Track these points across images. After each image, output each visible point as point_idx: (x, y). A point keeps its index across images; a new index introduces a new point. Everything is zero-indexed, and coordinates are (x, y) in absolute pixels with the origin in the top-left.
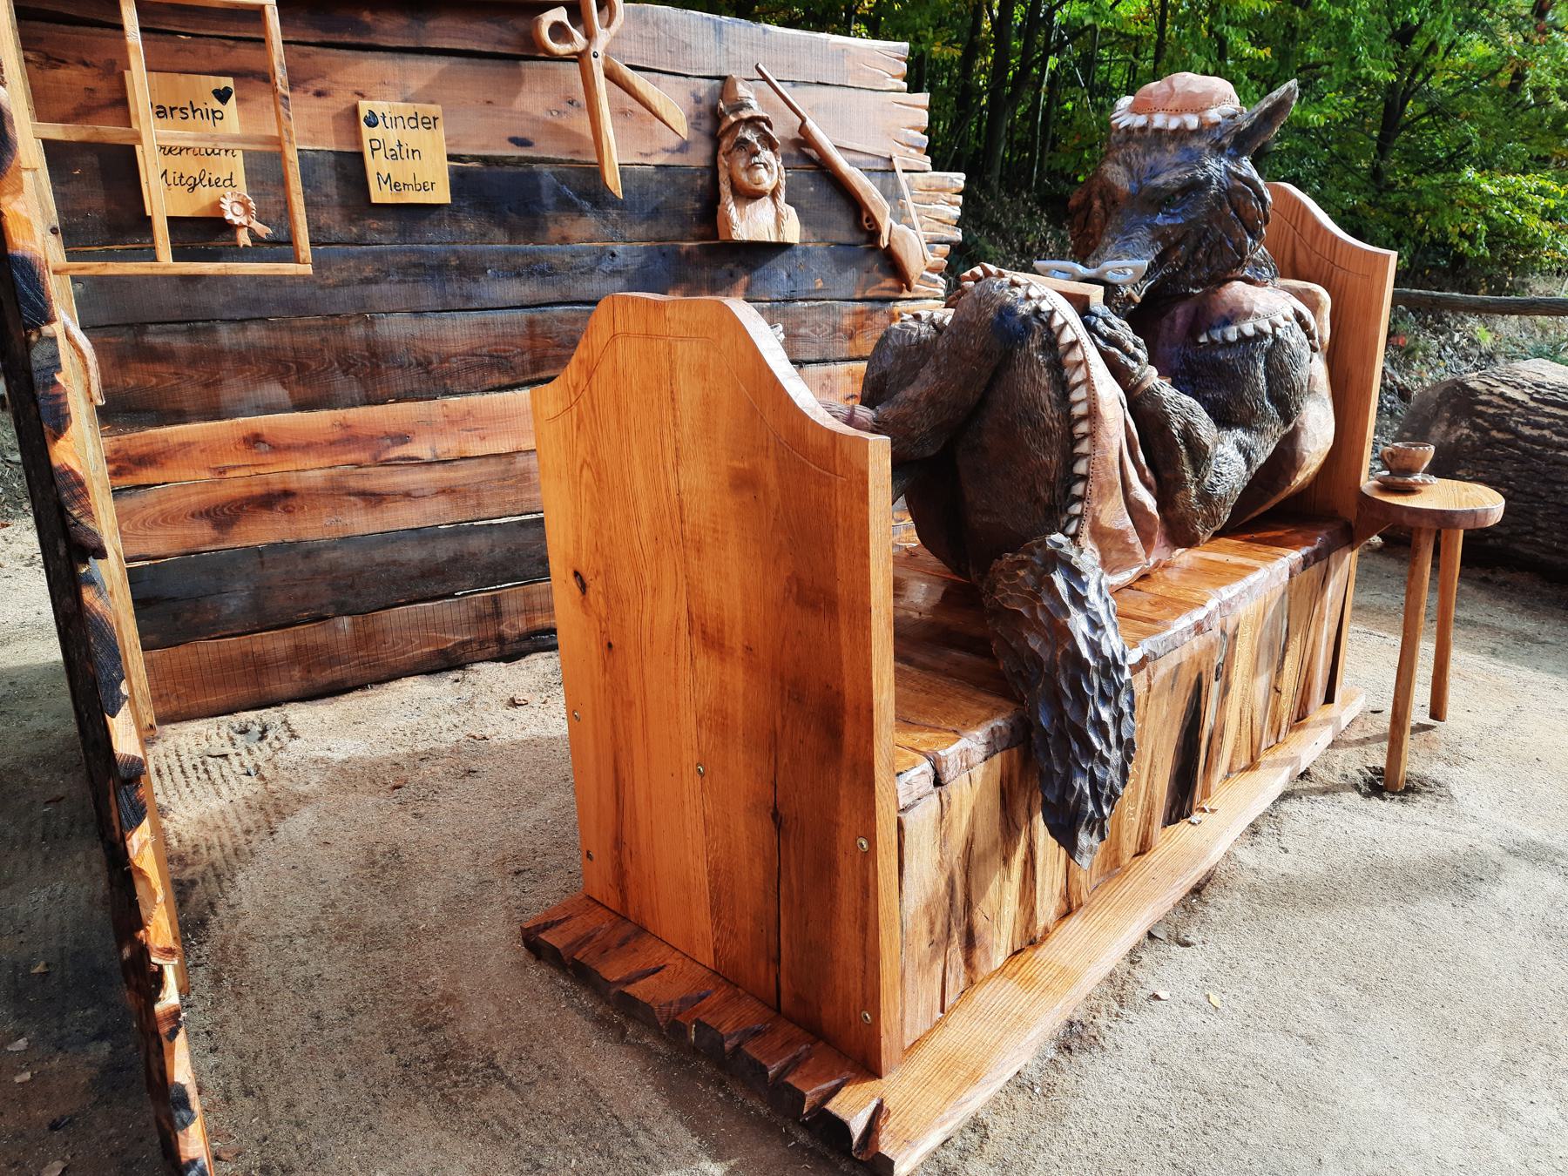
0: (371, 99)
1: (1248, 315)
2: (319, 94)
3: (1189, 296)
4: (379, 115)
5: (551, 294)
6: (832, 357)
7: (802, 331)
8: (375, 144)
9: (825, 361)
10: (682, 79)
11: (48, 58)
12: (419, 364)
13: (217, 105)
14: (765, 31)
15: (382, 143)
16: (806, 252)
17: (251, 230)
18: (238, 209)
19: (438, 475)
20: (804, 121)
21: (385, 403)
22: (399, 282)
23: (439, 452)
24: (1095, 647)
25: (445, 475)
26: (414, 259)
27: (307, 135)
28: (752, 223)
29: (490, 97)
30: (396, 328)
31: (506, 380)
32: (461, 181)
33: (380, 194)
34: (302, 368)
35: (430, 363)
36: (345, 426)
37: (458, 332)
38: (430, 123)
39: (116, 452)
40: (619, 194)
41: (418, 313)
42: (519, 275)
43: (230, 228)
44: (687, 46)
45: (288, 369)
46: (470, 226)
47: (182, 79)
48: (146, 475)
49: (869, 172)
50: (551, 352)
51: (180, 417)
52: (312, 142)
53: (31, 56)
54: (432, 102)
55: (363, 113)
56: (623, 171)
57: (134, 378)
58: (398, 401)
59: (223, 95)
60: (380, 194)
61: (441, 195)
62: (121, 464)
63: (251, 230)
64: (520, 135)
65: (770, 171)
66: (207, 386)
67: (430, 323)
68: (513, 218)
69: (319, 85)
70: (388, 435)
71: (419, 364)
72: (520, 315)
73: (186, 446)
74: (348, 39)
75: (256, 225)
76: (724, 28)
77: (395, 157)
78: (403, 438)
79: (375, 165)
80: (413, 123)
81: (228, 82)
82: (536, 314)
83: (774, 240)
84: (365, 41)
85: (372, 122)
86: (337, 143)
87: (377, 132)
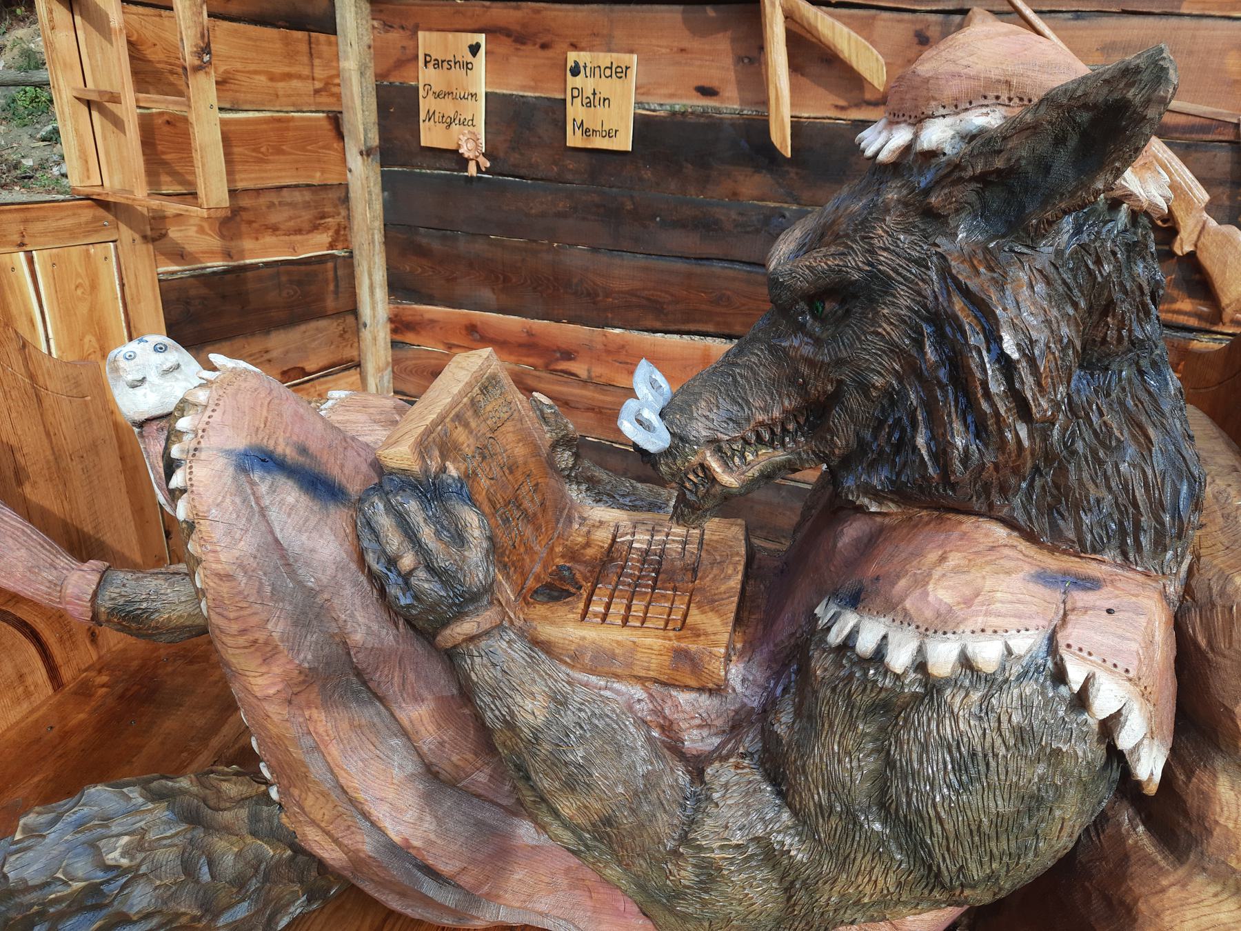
0: (582, 49)
1: (891, 608)
2: (544, 46)
3: (861, 510)
4: (581, 65)
5: (712, 249)
8: (576, 93)
10: (907, 16)
11: (385, 24)
12: (589, 294)
13: (469, 57)
15: (581, 91)
17: (478, 164)
18: (471, 145)
19: (588, 393)
21: (558, 321)
22: (584, 219)
23: (593, 375)
24: (905, 817)
25: (597, 396)
26: (597, 199)
27: (532, 84)
29: (685, 44)
30: (577, 258)
31: (658, 325)
32: (644, 126)
33: (574, 139)
34: (506, 280)
35: (597, 295)
36: (530, 334)
37: (624, 272)
38: (621, 72)
39: (396, 316)
40: (788, 153)
41: (595, 250)
42: (684, 226)
43: (463, 162)
45: (497, 278)
46: (647, 174)
47: (450, 35)
48: (410, 337)
50: (704, 307)
51: (430, 301)
52: (534, 89)
53: (376, 23)
54: (631, 52)
55: (570, 64)
56: (797, 127)
57: (408, 266)
58: (569, 322)
59: (474, 49)
60: (574, 139)
61: (624, 142)
62: (400, 326)
63: (478, 164)
64: (706, 83)
66: (448, 280)
67: (603, 259)
68: (689, 169)
69: (545, 39)
70: (559, 349)
71: (589, 294)
72: (680, 265)
73: (432, 322)
75: (482, 160)
77: (589, 105)
78: (568, 355)
79: (575, 111)
80: (608, 72)
81: (481, 38)
82: (697, 269)
85: (575, 72)
86: (743, 102)
87: (578, 81)
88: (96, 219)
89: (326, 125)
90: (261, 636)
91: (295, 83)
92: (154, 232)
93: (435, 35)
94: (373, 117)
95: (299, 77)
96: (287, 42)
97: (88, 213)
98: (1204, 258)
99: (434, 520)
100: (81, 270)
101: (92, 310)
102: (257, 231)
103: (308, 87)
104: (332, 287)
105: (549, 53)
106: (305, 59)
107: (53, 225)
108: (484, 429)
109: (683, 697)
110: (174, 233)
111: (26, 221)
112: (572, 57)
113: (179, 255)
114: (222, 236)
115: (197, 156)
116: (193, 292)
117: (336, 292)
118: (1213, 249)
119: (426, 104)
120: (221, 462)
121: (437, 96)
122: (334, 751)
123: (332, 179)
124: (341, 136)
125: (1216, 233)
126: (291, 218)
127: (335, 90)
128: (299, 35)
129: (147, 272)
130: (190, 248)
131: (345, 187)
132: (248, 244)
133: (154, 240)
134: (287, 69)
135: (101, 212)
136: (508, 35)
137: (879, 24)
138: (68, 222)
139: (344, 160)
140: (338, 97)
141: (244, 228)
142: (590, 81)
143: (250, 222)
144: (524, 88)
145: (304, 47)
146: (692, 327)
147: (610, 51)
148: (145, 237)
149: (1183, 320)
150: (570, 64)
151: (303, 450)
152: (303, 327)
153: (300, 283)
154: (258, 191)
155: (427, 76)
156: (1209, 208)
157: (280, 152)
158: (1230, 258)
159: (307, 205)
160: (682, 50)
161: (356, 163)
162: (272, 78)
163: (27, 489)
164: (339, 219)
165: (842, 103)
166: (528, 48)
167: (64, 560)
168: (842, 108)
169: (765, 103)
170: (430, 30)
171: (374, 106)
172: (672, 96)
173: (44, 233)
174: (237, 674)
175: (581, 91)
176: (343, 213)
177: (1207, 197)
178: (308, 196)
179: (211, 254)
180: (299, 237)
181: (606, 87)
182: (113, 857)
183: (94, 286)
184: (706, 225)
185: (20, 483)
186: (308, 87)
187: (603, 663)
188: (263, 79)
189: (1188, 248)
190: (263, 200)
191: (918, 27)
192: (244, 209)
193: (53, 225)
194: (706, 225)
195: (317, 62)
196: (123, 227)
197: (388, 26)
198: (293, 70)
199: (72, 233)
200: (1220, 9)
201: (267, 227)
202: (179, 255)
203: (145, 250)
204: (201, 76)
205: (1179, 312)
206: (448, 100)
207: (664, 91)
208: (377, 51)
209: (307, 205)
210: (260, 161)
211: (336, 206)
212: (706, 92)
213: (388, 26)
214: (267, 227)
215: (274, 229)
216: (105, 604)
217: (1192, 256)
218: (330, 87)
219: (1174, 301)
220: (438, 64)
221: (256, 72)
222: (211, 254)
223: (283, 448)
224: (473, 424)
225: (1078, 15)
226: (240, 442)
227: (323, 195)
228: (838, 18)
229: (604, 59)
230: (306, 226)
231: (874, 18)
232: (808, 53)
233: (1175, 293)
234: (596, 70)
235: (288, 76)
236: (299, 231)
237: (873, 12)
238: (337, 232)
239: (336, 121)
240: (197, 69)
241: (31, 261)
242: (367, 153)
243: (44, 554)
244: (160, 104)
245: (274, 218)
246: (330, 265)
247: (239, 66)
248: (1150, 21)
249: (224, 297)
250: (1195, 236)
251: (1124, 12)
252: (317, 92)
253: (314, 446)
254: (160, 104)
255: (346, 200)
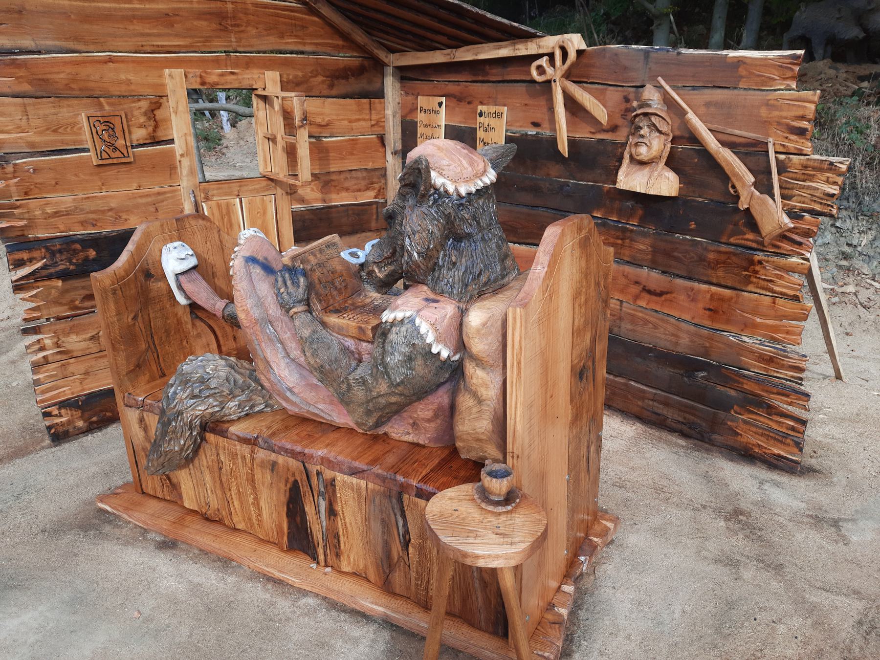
2: (469, 103)
6: (697, 277)
7: (676, 254)
9: (690, 279)
10: (620, 89)
13: (438, 108)
14: (679, 53)
15: (483, 124)
16: (686, 203)
20: (685, 113)
28: (631, 180)
29: (526, 102)
31: (515, 239)
38: (499, 115)
44: (625, 68)
49: (743, 157)
52: (464, 123)
54: (505, 105)
56: (572, 142)
59: (440, 104)
64: (535, 121)
65: (654, 145)
72: (525, 210)
74: (480, 78)
76: (652, 55)
77: (486, 131)
81: (444, 99)
83: (642, 191)
84: (485, 79)
85: (481, 115)
88: (267, 185)
89: (376, 141)
90: (245, 308)
91: (362, 123)
92: (291, 191)
93: (425, 98)
94: (399, 136)
95: (364, 120)
96: (359, 105)
97: (265, 183)
98: (752, 210)
99: (291, 279)
100: (260, 206)
101: (263, 223)
102: (338, 190)
103: (369, 124)
104: (375, 217)
105: (471, 106)
106: (368, 112)
107: (250, 187)
108: (323, 258)
109: (364, 344)
110: (300, 191)
111: (240, 186)
112: (480, 108)
113: (302, 201)
114: (322, 193)
115: (299, 161)
116: (307, 217)
117: (377, 219)
118: (757, 207)
119: (420, 130)
120: (242, 260)
121: (425, 126)
122: (263, 345)
123: (378, 165)
124: (384, 145)
125: (759, 198)
126: (355, 184)
127: (382, 124)
128: (365, 101)
129: (287, 208)
130: (307, 197)
131: (385, 169)
132: (334, 196)
133: (291, 194)
134: (358, 117)
135: (270, 182)
136: (455, 98)
137: (608, 92)
138: (256, 187)
139: (385, 157)
140: (384, 127)
141: (332, 189)
142: (487, 119)
143: (335, 186)
144: (460, 122)
145: (368, 106)
146: (527, 241)
147: (496, 105)
148: (287, 193)
149: (749, 244)
150: (479, 111)
151: (266, 259)
152: (359, 235)
153: (358, 215)
154: (340, 172)
155: (421, 117)
156: (755, 185)
157: (352, 154)
158: (765, 212)
159: (364, 178)
160: (526, 105)
161: (390, 157)
162: (350, 121)
163: (216, 280)
164: (380, 185)
165: (593, 130)
166: (463, 103)
167: (216, 298)
168: (593, 133)
169: (555, 130)
170: (423, 95)
171: (400, 131)
172: (521, 126)
173: (246, 191)
174: (465, 555)
175: (483, 124)
176: (383, 181)
177: (753, 179)
178: (365, 174)
179: (316, 200)
180: (359, 193)
181: (493, 122)
182: (208, 370)
183: (265, 213)
184: (535, 190)
185: (214, 278)
186: (369, 124)
187: (340, 330)
188: (346, 122)
189: (746, 206)
190: (342, 176)
191: (625, 94)
192: (333, 180)
193: (250, 187)
194: (535, 190)
195: (373, 112)
196: (278, 188)
197: (407, 94)
198: (360, 117)
199: (257, 191)
200: (756, 85)
201: (344, 189)
202: (302, 201)
203: (286, 198)
204: (302, 129)
205: (747, 240)
206: (429, 128)
207: (518, 124)
208: (402, 105)
209: (364, 178)
210: (342, 159)
211: (379, 178)
212: (536, 125)
213: (407, 94)
214: (344, 189)
215: (347, 189)
216: (226, 313)
217: (748, 209)
218: (380, 123)
219: (745, 234)
220: (426, 112)
221: (343, 120)
222: (316, 200)
223: (260, 258)
224: (318, 256)
225: (694, 88)
226: (248, 255)
227: (373, 173)
228: (584, 89)
229: (493, 109)
230: (363, 188)
231: (606, 89)
232: (573, 106)
233: (745, 229)
234: (489, 115)
235: (359, 120)
236: (359, 190)
237: (605, 87)
238: (379, 191)
239: (382, 139)
240: (300, 127)
241: (241, 202)
242: (395, 153)
243: (212, 296)
244: (291, 139)
245: (346, 185)
246: (374, 206)
247: (335, 118)
248: (726, 91)
249: (321, 219)
250: (748, 200)
251: (714, 87)
252: (372, 126)
253: (269, 258)
254: (291, 139)
255: (385, 175)
